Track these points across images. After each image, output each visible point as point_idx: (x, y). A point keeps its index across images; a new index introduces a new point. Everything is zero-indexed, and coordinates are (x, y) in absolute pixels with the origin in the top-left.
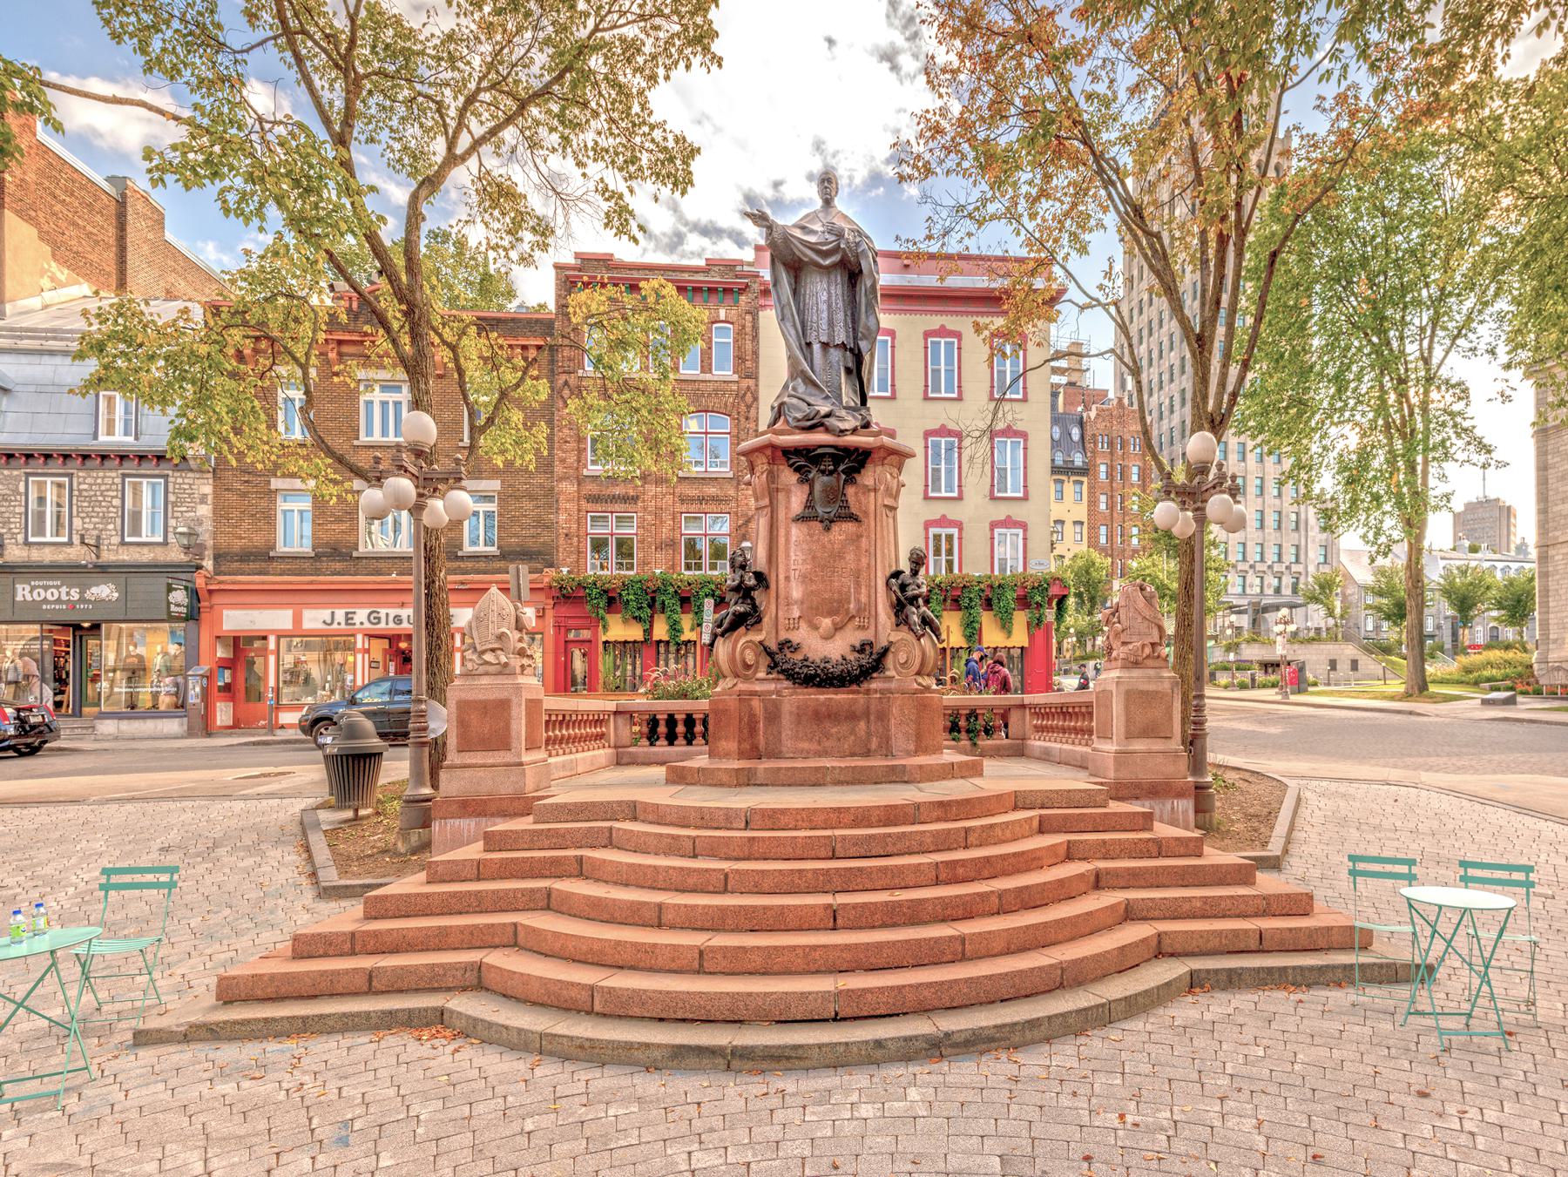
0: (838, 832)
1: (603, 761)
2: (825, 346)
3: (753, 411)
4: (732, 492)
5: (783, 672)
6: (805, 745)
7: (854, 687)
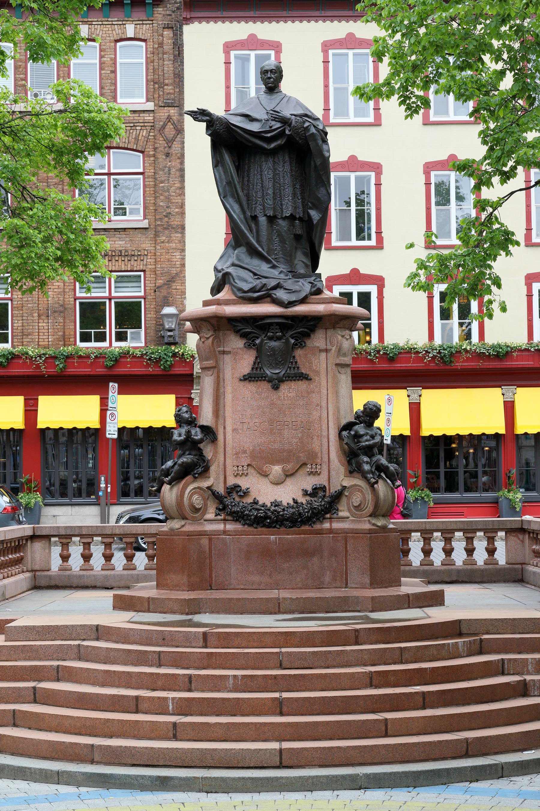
0: (284, 650)
1: (25, 585)
2: (271, 219)
3: (176, 146)
4: (147, 245)
5: (231, 514)
6: (256, 578)
7: (306, 528)
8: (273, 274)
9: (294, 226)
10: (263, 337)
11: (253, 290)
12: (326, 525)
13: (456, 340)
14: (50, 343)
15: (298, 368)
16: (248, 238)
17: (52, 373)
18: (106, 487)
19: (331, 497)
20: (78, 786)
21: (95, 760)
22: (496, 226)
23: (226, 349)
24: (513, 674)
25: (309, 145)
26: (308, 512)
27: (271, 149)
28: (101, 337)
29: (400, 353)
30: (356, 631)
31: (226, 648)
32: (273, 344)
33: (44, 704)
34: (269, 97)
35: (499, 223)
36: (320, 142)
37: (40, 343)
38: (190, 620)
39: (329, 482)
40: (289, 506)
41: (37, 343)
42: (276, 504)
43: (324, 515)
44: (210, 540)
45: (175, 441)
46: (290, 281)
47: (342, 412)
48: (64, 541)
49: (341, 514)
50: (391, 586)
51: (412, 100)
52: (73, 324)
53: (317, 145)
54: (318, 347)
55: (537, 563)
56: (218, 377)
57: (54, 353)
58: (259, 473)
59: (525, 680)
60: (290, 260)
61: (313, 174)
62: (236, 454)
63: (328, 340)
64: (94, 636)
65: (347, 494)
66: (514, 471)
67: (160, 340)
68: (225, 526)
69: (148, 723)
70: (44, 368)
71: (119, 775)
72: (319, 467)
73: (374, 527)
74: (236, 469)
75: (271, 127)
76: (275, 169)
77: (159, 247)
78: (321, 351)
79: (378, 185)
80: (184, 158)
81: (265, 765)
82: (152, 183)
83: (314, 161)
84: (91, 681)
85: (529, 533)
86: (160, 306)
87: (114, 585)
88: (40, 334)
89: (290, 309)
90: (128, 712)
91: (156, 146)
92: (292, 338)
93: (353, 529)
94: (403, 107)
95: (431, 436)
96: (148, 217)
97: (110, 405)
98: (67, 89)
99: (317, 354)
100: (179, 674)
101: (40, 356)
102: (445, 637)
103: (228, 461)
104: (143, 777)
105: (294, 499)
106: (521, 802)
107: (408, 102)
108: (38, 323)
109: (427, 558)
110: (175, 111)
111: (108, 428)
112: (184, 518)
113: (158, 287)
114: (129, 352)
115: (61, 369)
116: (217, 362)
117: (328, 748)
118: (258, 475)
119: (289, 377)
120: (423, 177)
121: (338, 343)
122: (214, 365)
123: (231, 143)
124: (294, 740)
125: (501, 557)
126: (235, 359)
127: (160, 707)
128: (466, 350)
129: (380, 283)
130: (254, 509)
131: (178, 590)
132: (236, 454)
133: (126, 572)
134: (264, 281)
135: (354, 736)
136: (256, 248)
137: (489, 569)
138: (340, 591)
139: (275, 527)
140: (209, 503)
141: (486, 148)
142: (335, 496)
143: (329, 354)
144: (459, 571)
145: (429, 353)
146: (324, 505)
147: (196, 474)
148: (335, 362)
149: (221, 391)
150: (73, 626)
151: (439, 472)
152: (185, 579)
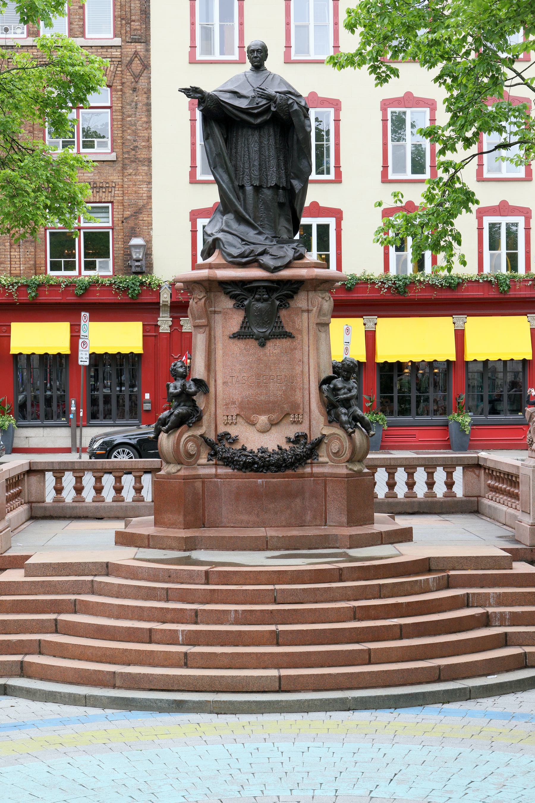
0: (278, 587)
1: (24, 517)
2: (257, 189)
3: (142, 81)
4: (115, 177)
5: (222, 459)
6: (245, 517)
7: (289, 472)
8: (259, 240)
9: (278, 195)
11: (242, 255)
12: (308, 470)
14: (22, 272)
15: (283, 327)
16: (235, 206)
17: (24, 301)
18: (78, 411)
19: (312, 444)
20: (104, 708)
21: (117, 685)
22: (458, 185)
24: (477, 607)
26: (291, 458)
27: (258, 124)
28: (70, 266)
29: (357, 284)
30: (340, 569)
31: (226, 585)
32: (259, 305)
33: (65, 634)
36: (303, 118)
37: (12, 272)
38: (189, 557)
39: (310, 430)
40: (274, 452)
41: (9, 272)
42: (263, 451)
43: (305, 461)
44: (203, 483)
45: (172, 393)
46: (275, 247)
47: (322, 367)
48: (58, 475)
49: (321, 459)
50: (365, 524)
51: (382, 70)
52: (44, 253)
53: (300, 120)
54: (301, 308)
55: (492, 497)
56: (210, 334)
57: (27, 282)
58: (247, 422)
59: (488, 612)
60: (274, 228)
61: (295, 147)
62: (227, 404)
63: (310, 301)
65: (326, 441)
66: (463, 396)
67: (127, 269)
68: (216, 471)
69: (162, 653)
70: (16, 297)
71: (140, 699)
72: (300, 417)
73: (351, 472)
74: (226, 418)
75: (257, 104)
76: (261, 143)
78: (303, 311)
79: (337, 121)
80: (150, 93)
81: (267, 690)
83: (297, 135)
85: (485, 469)
86: (128, 236)
87: (104, 515)
88: (12, 263)
90: (142, 642)
91: (124, 80)
92: (277, 300)
93: (332, 473)
94: (374, 76)
95: (386, 362)
96: (116, 150)
97: (82, 333)
98: (51, 42)
99: (300, 313)
100: (186, 609)
101: (12, 285)
102: (417, 574)
103: (219, 411)
104: (161, 701)
105: (278, 446)
106: (488, 721)
107: (378, 71)
108: (10, 252)
109: (391, 491)
110: (142, 47)
111: (80, 356)
112: (180, 463)
113: (126, 219)
114: (98, 281)
115: (33, 297)
117: (321, 675)
118: (246, 424)
119: (274, 335)
120: (380, 113)
121: (318, 304)
122: (206, 323)
123: (218, 117)
124: (290, 668)
125: (459, 491)
126: (225, 318)
127: (171, 638)
128: (419, 281)
129: (338, 216)
130: (243, 455)
131: (174, 528)
132: (226, 405)
133: (115, 504)
134: (252, 247)
135: (342, 664)
136: (244, 216)
137: (448, 501)
139: (262, 471)
141: (450, 115)
142: (316, 443)
143: (311, 315)
144: (420, 503)
145: (385, 283)
146: (305, 452)
147: (190, 423)
148: (316, 322)
149: (213, 347)
150: (85, 563)
152: (181, 519)
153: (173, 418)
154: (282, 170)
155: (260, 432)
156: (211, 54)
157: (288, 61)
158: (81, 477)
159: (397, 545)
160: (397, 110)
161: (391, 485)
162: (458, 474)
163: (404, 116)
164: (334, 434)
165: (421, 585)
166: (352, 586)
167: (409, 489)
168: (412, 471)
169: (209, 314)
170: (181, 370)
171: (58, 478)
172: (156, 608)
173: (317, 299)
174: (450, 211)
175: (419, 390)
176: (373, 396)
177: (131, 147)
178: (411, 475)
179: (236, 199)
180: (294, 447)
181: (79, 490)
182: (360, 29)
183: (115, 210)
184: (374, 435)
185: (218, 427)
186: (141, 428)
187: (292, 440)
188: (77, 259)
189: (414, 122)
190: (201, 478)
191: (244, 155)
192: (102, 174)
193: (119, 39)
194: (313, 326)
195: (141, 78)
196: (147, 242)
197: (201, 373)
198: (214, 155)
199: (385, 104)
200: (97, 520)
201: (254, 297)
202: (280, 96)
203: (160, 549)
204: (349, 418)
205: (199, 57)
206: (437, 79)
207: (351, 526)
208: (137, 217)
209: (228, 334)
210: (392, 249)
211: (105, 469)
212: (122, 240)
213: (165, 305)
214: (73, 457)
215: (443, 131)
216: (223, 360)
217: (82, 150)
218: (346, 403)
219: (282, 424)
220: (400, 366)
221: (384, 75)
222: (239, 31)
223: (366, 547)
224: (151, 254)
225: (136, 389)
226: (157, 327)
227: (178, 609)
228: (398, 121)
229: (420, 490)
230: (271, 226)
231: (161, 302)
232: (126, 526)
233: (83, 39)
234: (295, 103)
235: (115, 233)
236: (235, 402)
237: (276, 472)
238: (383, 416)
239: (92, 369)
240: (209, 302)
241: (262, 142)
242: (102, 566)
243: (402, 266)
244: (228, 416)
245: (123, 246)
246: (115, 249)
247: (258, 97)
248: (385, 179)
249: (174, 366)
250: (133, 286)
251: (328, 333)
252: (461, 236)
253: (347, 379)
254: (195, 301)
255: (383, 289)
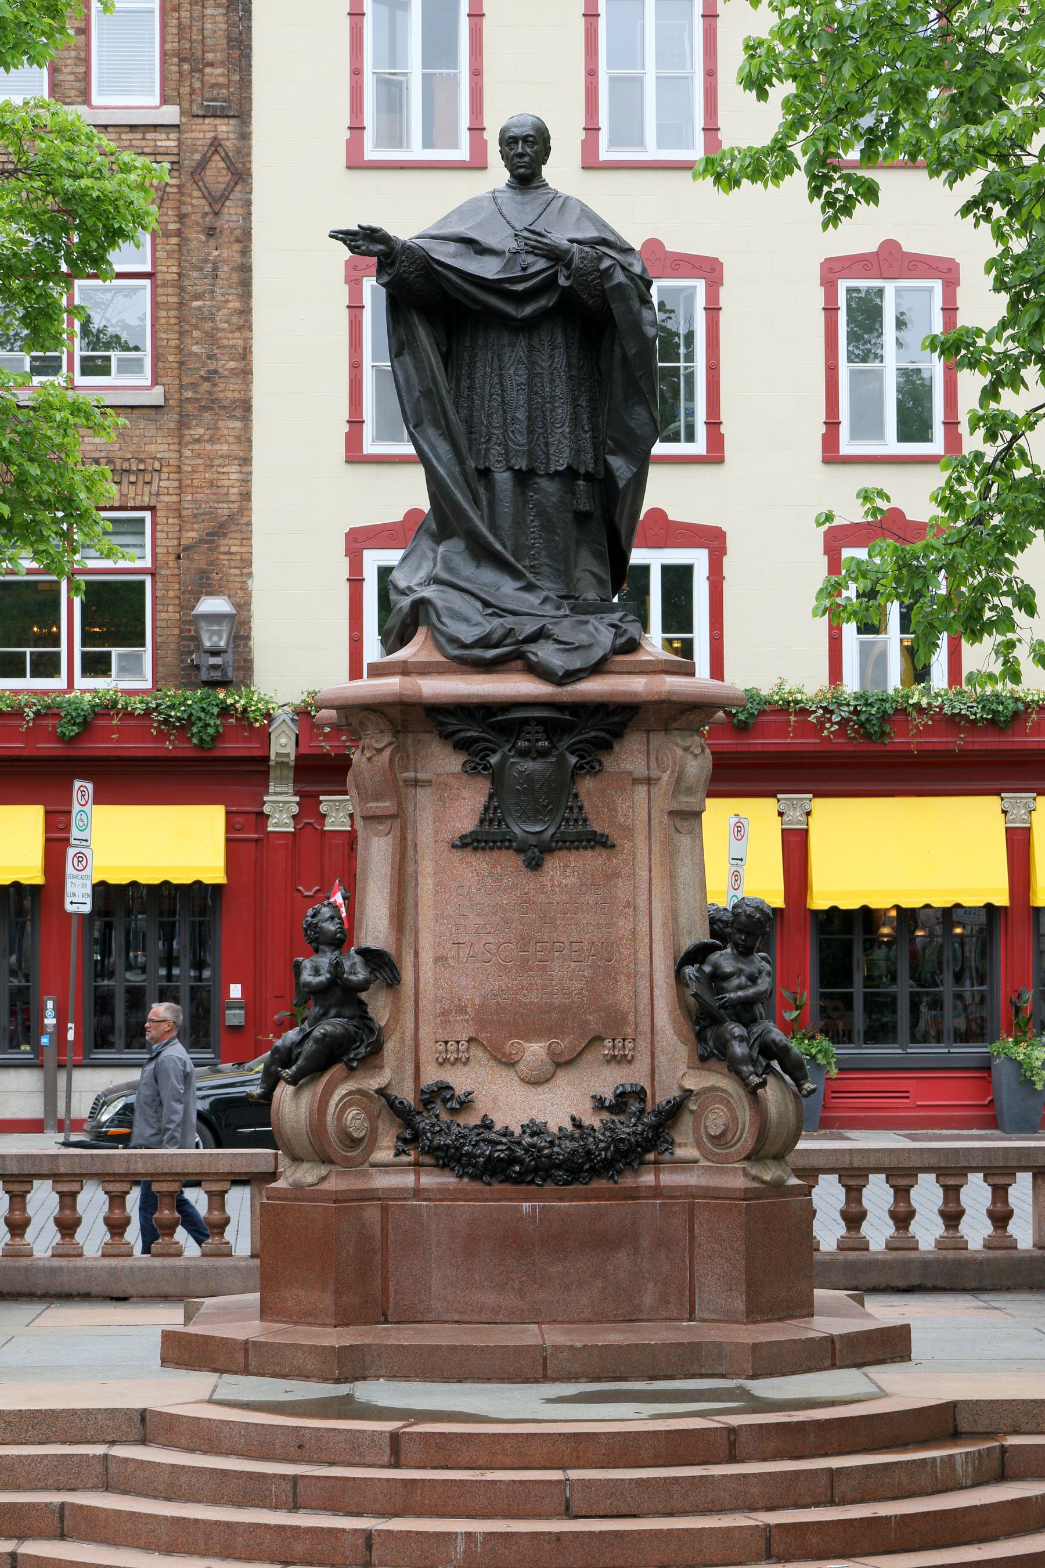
0: (574, 1474)
2: (523, 478)
3: (231, 211)
4: (161, 447)
5: (432, 1150)
6: (489, 1298)
7: (601, 1184)
8: (528, 604)
9: (573, 494)
10: (506, 749)
11: (484, 642)
12: (648, 1179)
13: (894, 680)
15: (585, 820)
16: (469, 520)
18: (61, 1028)
19: (658, 1113)
23: (421, 776)
25: (611, 310)
26: (606, 1149)
27: (523, 319)
28: (47, 666)
29: (762, 713)
30: (731, 1430)
31: (442, 1468)
32: (528, 766)
34: (519, 198)
35: (1027, 465)
36: (636, 304)
38: (349, 1398)
39: (653, 1080)
42: (535, 1130)
43: (641, 1155)
44: (384, 1209)
45: (307, 985)
46: (566, 622)
47: (683, 921)
48: (16, 1188)
49: (680, 1153)
53: (630, 309)
54: (631, 773)
56: (403, 838)
58: (495, 1058)
60: (565, 574)
61: (618, 375)
63: (653, 757)
64: (135, 1433)
65: (694, 1108)
66: (1029, 995)
67: (190, 674)
68: (417, 1180)
73: (755, 1185)
74: (442, 1048)
75: (524, 269)
76: (532, 364)
77: (188, 453)
78: (636, 781)
79: (713, 310)
80: (250, 240)
82: (174, 299)
83: (622, 346)
84: (142, 1541)
86: (191, 592)
87: (130, 1290)
89: (569, 688)
92: (573, 753)
95: (834, 909)
96: (164, 380)
97: (75, 833)
99: (628, 787)
100: (343, 1530)
102: (924, 1443)
103: (425, 1030)
105: (573, 1119)
107: (826, 189)
109: (853, 1234)
111: (69, 889)
112: (326, 1160)
113: (186, 549)
114: (115, 702)
116: (400, 804)
118: (492, 1063)
119: (564, 842)
120: (821, 291)
121: (675, 764)
122: (393, 811)
123: (428, 302)
125: (1023, 1232)
126: (441, 798)
128: (917, 706)
129: (715, 544)
130: (484, 1140)
131: (311, 1324)
132: (443, 1014)
134: (509, 621)
136: (490, 545)
138: (678, 1328)
139: (532, 1182)
140: (381, 1126)
141: (1004, 298)
142: (667, 1111)
143: (655, 790)
144: (926, 1264)
145: (832, 712)
146: (642, 1133)
147: (353, 1060)
149: (410, 870)
150: (88, 1412)
151: (851, 994)
152: (328, 1300)
153: (309, 1046)
154: (586, 432)
155: (528, 1083)
156: (401, 147)
157: (591, 163)
158: (74, 1195)
159: (871, 1370)
160: (863, 284)
161: (854, 1218)
162: (1022, 1190)
163: (878, 301)
164: (713, 1089)
165: (935, 1472)
166: (760, 1474)
167: (898, 1229)
168: (905, 1182)
169: (400, 787)
170: (331, 927)
171: (16, 1196)
172: (267, 1526)
173: (670, 750)
174: (1004, 534)
175: (915, 976)
176: (802, 994)
177: (202, 373)
178: (902, 1193)
179: (469, 502)
180: (613, 1122)
181: (67, 1226)
182: (783, 89)
183: (159, 528)
184: (813, 1091)
185: (422, 1069)
186: (219, 1071)
187: (607, 1104)
188: (63, 649)
189: (902, 314)
190: (379, 1199)
191: (491, 395)
192: (128, 439)
193: (176, 109)
194: (660, 819)
195: (228, 203)
196: (237, 606)
197: (381, 936)
198: (417, 394)
199: (832, 271)
200: (114, 1303)
201: (513, 746)
202: (581, 251)
203: (274, 1375)
204: (751, 1048)
205: (370, 153)
206: (966, 209)
207: (756, 1322)
208: (215, 544)
209: (448, 836)
210: (849, 629)
211: (134, 1174)
212: (177, 602)
213: (282, 765)
214: (46, 1144)
215: (989, 341)
216: (433, 900)
217: (80, 380)
218: (745, 1011)
219: (582, 1063)
220: (867, 916)
221: (841, 197)
222: (472, 89)
223: (793, 1373)
224: (248, 638)
225: (206, 973)
226: (262, 818)
227: (323, 1529)
228: (863, 312)
229: (927, 1231)
230: (557, 570)
231: (273, 757)
232: (188, 1318)
233: (85, 108)
234: (618, 268)
235: (159, 585)
236: (466, 1006)
237: (567, 1183)
238: (826, 1043)
239: (98, 923)
240: (401, 758)
241: (537, 364)
242: (131, 1419)
243: (876, 666)
244: (446, 1043)
245: (177, 616)
246: (158, 623)
247: (527, 252)
248: (831, 454)
249: (314, 916)
250: (203, 715)
251: (697, 835)
252: (1033, 593)
253: (744, 952)
254: (368, 754)
255: (828, 725)
